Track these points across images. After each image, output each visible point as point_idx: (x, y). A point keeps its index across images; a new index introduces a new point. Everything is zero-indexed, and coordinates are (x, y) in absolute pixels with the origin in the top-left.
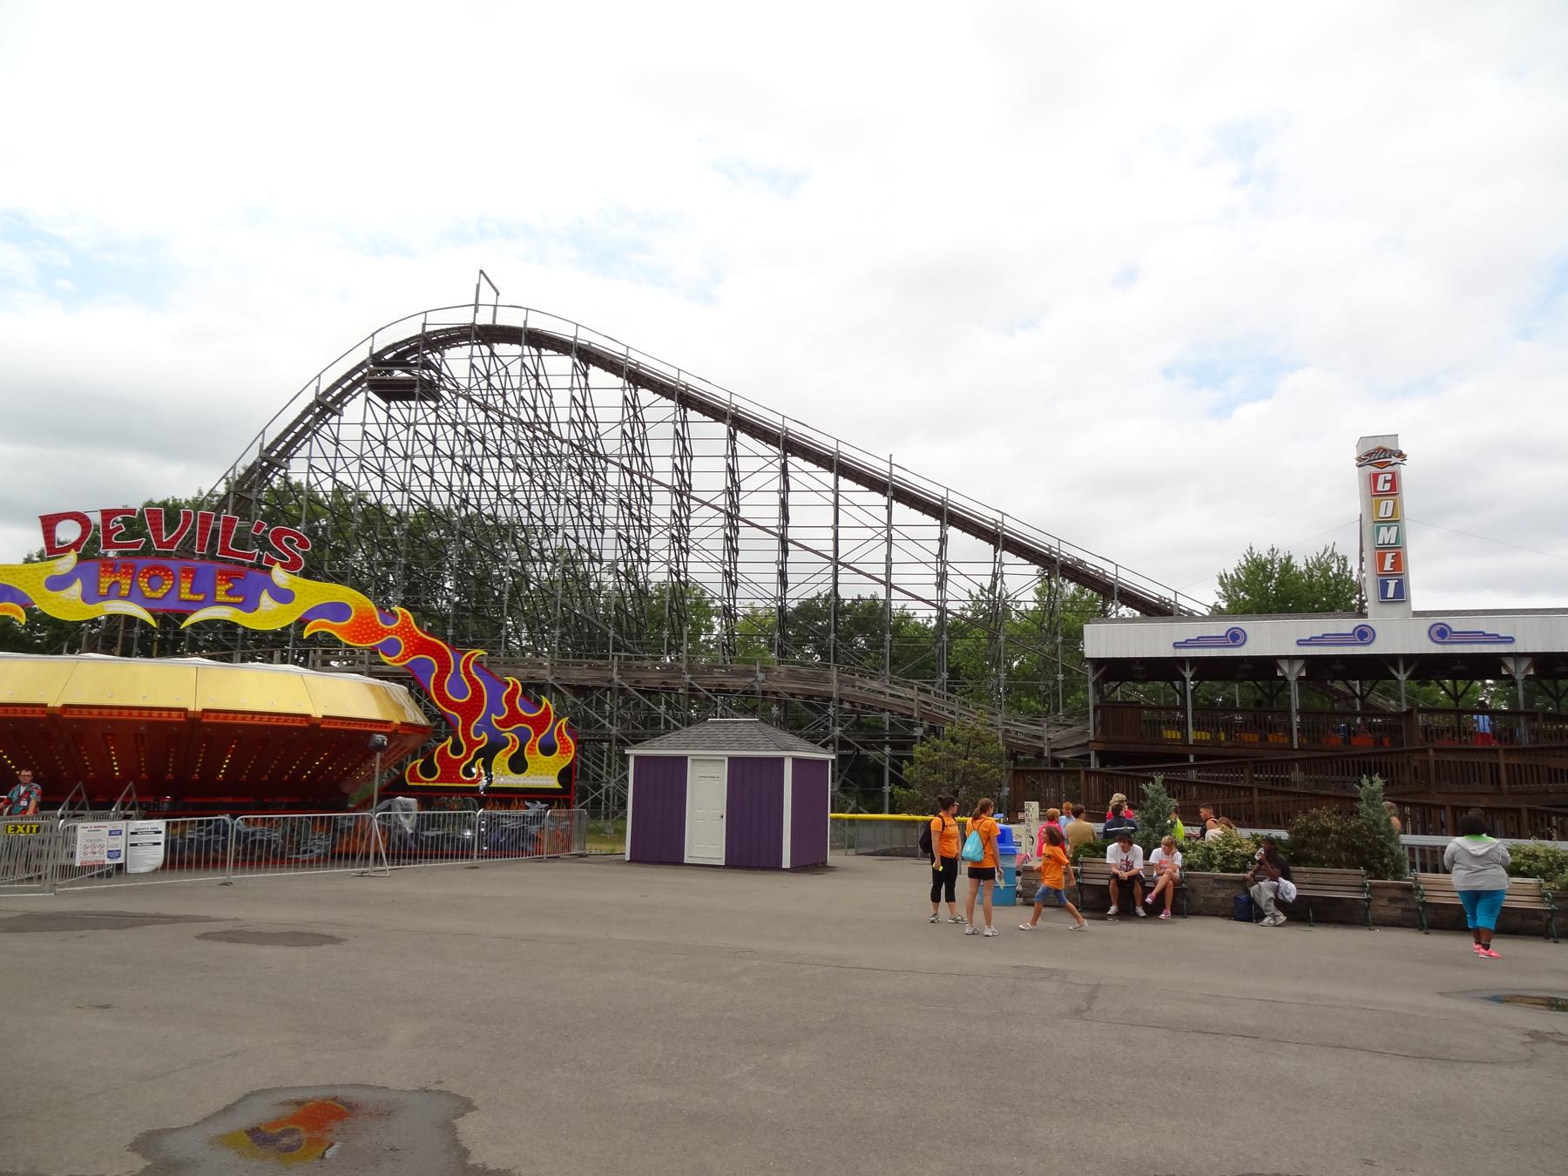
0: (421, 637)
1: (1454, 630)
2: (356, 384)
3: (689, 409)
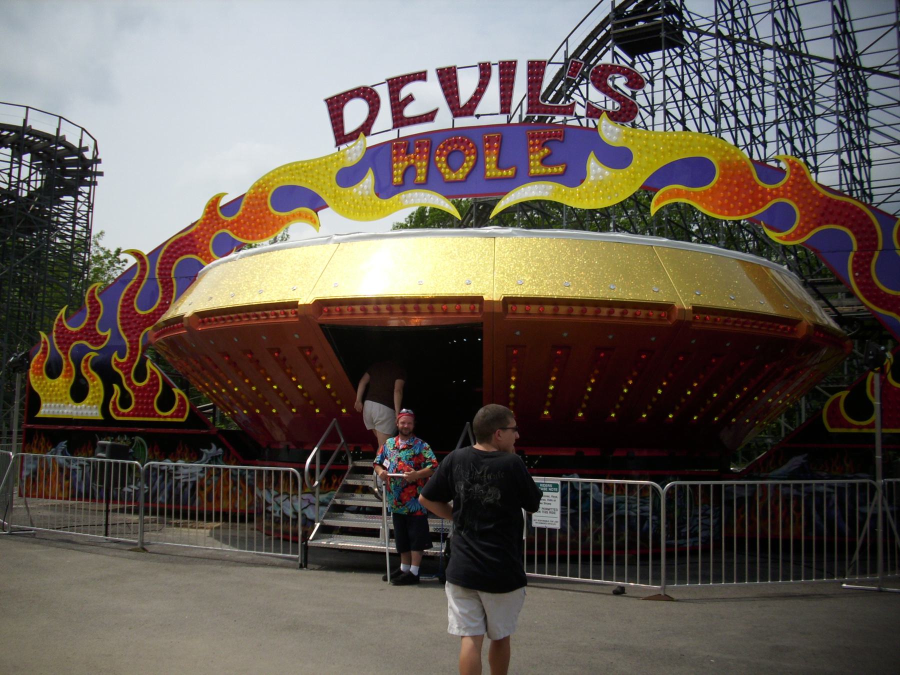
0: (824, 197)
2: (601, 43)
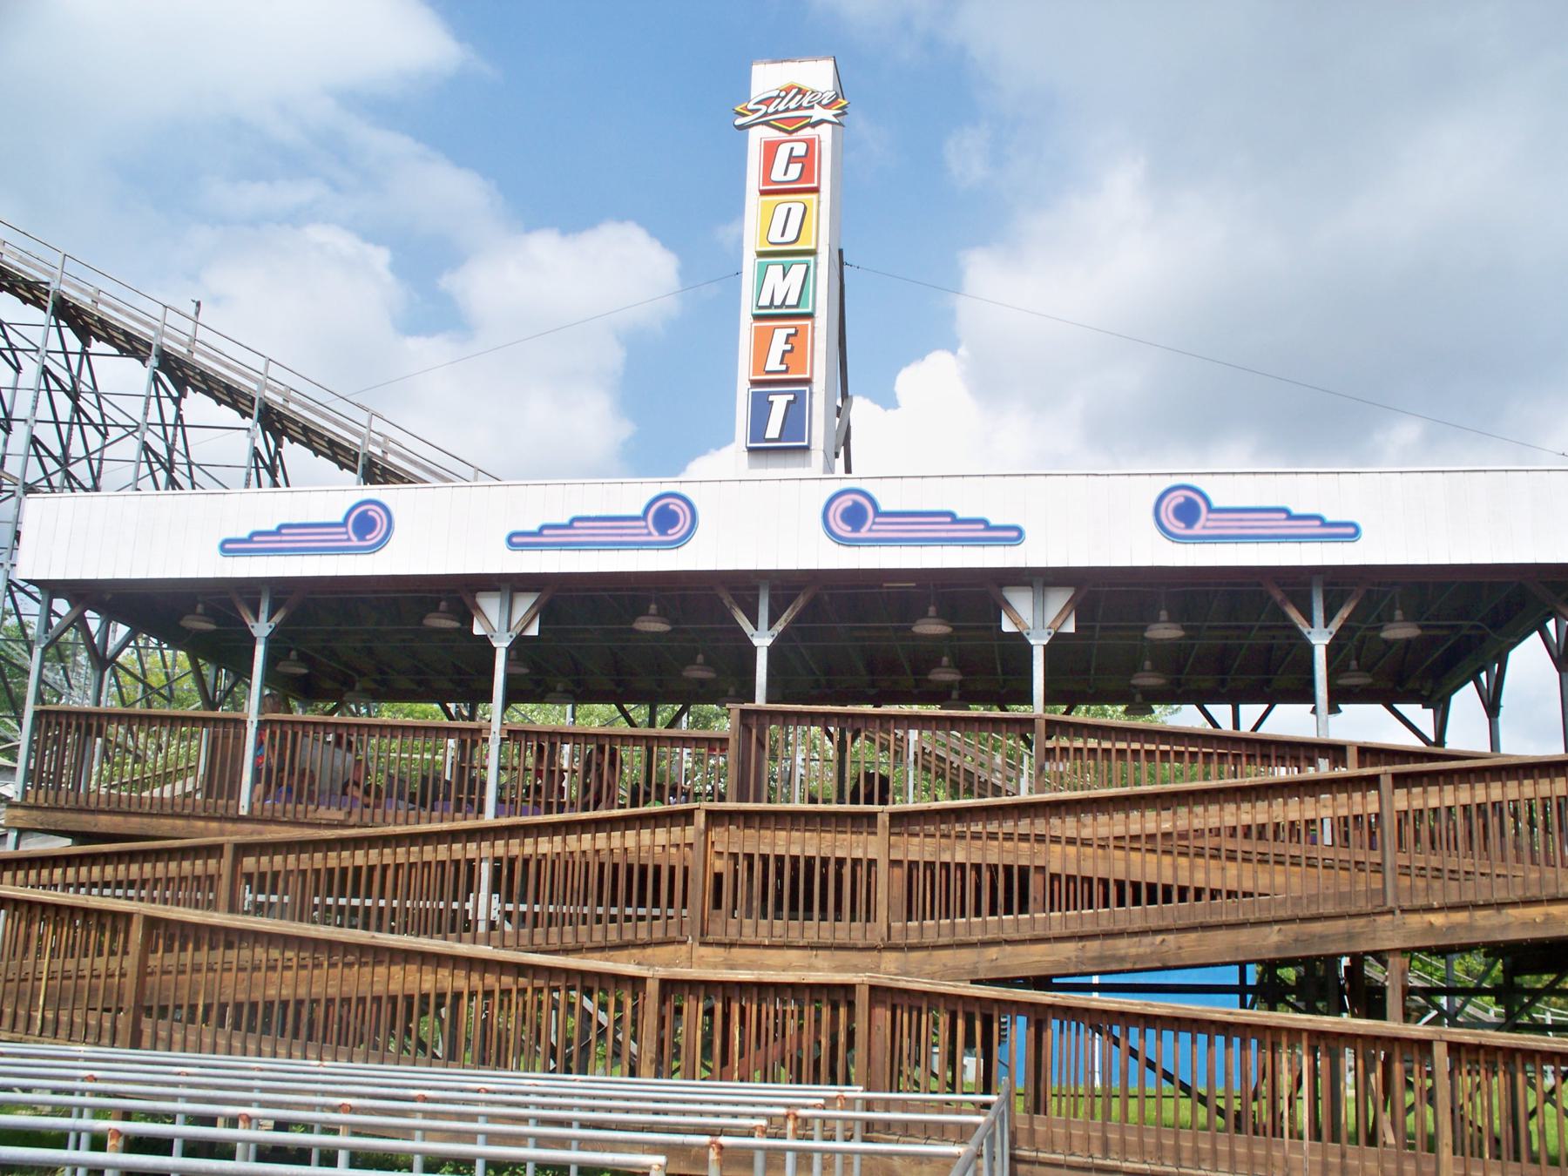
1: (884, 507)
3: (286, 440)
